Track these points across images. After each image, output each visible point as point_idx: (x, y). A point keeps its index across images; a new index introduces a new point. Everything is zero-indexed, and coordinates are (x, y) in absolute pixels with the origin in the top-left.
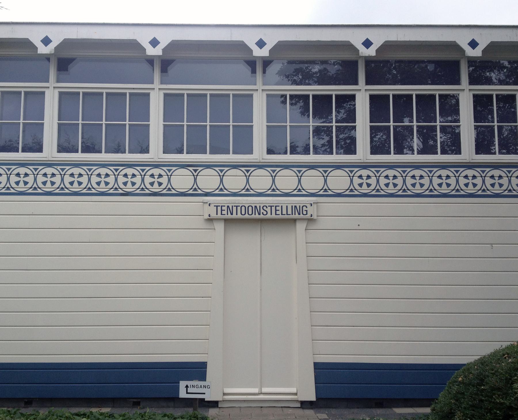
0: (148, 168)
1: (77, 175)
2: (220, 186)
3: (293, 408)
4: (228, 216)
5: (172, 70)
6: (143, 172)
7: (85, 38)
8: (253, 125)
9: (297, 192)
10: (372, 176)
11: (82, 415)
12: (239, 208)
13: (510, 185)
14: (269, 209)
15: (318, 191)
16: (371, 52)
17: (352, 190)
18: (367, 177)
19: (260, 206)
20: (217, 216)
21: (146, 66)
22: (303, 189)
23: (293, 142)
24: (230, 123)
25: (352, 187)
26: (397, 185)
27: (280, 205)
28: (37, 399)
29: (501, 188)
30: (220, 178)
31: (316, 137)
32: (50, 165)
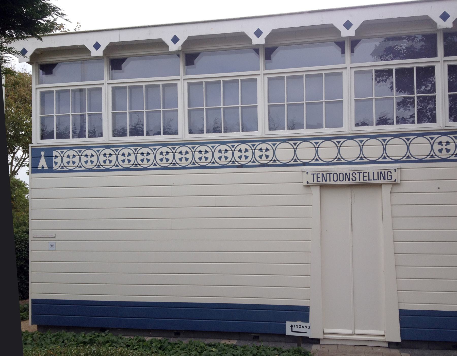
0: (257, 143)
1: (264, 149)
2: (79, 164)
3: (381, 348)
4: (322, 182)
5: (276, 56)
6: (253, 147)
7: (204, 34)
8: (343, 101)
9: (430, 157)
10: (451, 142)
11: (213, 345)
12: (332, 175)
13: (62, 163)
14: (357, 176)
15: (426, 157)
16: (449, 24)
17: (361, 158)
18: (446, 143)
19: (350, 173)
20: (314, 183)
21: (254, 54)
22: (342, 158)
23: (385, 116)
24: (323, 100)
25: (432, 153)
26: (450, 150)
27: (367, 172)
28: (184, 331)
29: (111, 164)
30: (316, 149)
31: (403, 108)
32: (184, 145)
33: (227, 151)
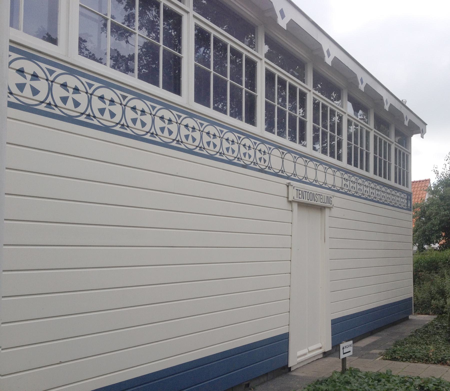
10: (82, 91)
12: (306, 193)
29: (143, 128)
33: (37, 76)
